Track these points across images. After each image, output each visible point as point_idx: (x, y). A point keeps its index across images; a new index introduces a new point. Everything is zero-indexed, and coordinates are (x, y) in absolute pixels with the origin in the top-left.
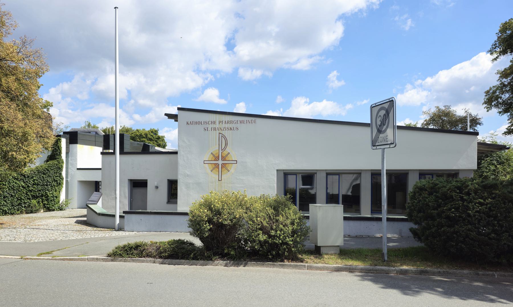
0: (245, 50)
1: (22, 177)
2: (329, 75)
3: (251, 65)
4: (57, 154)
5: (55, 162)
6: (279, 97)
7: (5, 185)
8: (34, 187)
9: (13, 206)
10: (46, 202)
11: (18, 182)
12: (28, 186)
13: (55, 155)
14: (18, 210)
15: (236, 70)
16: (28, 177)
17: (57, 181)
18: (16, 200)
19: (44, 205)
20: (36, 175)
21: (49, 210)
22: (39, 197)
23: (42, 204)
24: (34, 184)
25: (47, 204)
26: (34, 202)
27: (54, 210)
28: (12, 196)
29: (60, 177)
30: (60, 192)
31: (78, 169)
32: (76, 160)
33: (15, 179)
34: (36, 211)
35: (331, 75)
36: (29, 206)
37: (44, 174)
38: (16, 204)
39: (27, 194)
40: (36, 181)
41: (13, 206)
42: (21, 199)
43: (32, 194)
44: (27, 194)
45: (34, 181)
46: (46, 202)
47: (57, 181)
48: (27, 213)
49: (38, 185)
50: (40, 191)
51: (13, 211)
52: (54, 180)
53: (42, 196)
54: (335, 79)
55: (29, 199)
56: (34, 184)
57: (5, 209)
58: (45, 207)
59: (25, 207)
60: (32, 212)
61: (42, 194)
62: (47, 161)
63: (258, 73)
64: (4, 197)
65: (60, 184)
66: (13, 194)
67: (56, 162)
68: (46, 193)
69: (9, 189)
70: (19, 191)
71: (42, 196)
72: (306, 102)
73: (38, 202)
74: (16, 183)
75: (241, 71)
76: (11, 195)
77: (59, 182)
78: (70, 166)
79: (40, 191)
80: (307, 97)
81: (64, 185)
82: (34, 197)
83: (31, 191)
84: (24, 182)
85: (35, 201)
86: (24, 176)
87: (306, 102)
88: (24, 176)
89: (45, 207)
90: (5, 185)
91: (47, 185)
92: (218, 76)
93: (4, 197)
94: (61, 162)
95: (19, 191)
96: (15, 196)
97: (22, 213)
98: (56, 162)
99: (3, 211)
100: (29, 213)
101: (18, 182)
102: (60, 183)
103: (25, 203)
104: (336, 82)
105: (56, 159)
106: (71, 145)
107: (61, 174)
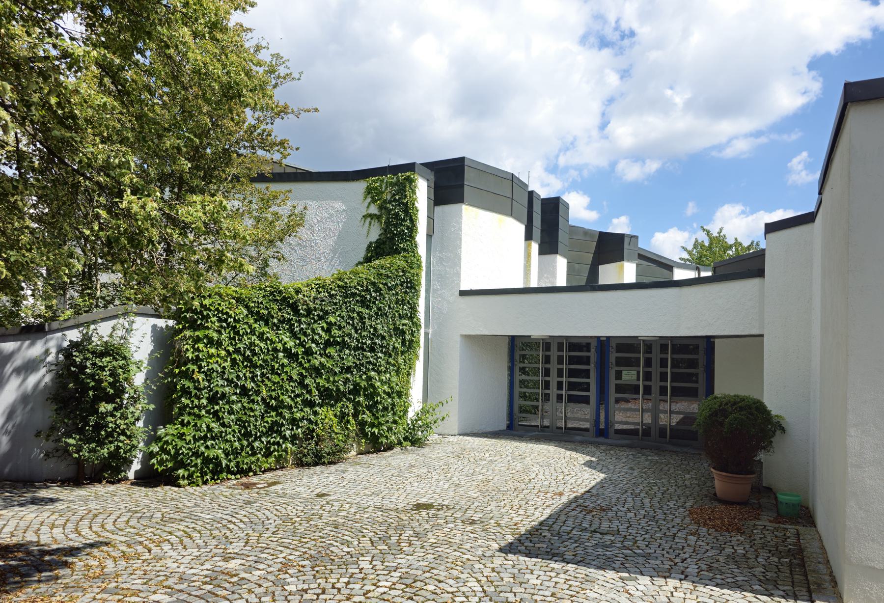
0: (626, 132)
1: (287, 314)
2: (790, 161)
3: (638, 156)
4: (401, 234)
5: (399, 261)
6: (691, 204)
7: (219, 344)
8: (329, 357)
9: (247, 435)
10: (367, 417)
11: (270, 334)
12: (308, 352)
13: (393, 236)
14: (268, 454)
15: (613, 165)
16: (309, 311)
17: (403, 333)
18: (259, 408)
19: (362, 424)
20: (338, 307)
21: (376, 446)
22: (344, 394)
23: (353, 426)
24: (328, 344)
25: (372, 425)
26: (327, 415)
27: (390, 447)
28: (244, 391)
29: (411, 318)
30: (409, 374)
31: (463, 293)
32: (456, 261)
33: (259, 317)
34: (334, 457)
35: (795, 161)
36: (309, 434)
37: (364, 303)
38: (262, 427)
39: (301, 384)
40: (335, 332)
41: (247, 435)
42: (281, 405)
43: (321, 382)
44: (301, 384)
45: (328, 331)
46: (367, 417)
47: (403, 333)
48: (300, 464)
49: (344, 345)
50: (349, 370)
51: (246, 460)
52: (396, 329)
53: (356, 391)
54: (800, 167)
55: (311, 404)
56: (328, 344)
57: (211, 454)
58: (365, 435)
59: (294, 437)
60: (318, 460)
61: (356, 385)
62: (368, 260)
63: (653, 166)
64: (213, 400)
65: (410, 346)
66: (250, 385)
67: (402, 264)
68: (370, 378)
69: (234, 363)
70: (273, 371)
71: (356, 391)
72: (743, 212)
73: (342, 417)
74: (261, 336)
75: (622, 165)
76: (243, 387)
77: (408, 337)
78: (435, 285)
79: (349, 370)
80: (744, 205)
81: (421, 352)
82: (329, 396)
83: (317, 371)
84: (294, 335)
85: (331, 414)
86: (296, 311)
87: (743, 212)
88: (296, 311)
89: (365, 435)
90: (219, 344)
91: (372, 350)
92: (585, 173)
93: (213, 400)
94: (413, 264)
95: (273, 371)
96: (258, 393)
97: (280, 464)
98: (402, 264)
99: (207, 461)
100: (308, 465)
101: (270, 334)
102: (411, 341)
103: (294, 422)
104: (804, 173)
105: (397, 252)
106: (438, 209)
107: (413, 308)
